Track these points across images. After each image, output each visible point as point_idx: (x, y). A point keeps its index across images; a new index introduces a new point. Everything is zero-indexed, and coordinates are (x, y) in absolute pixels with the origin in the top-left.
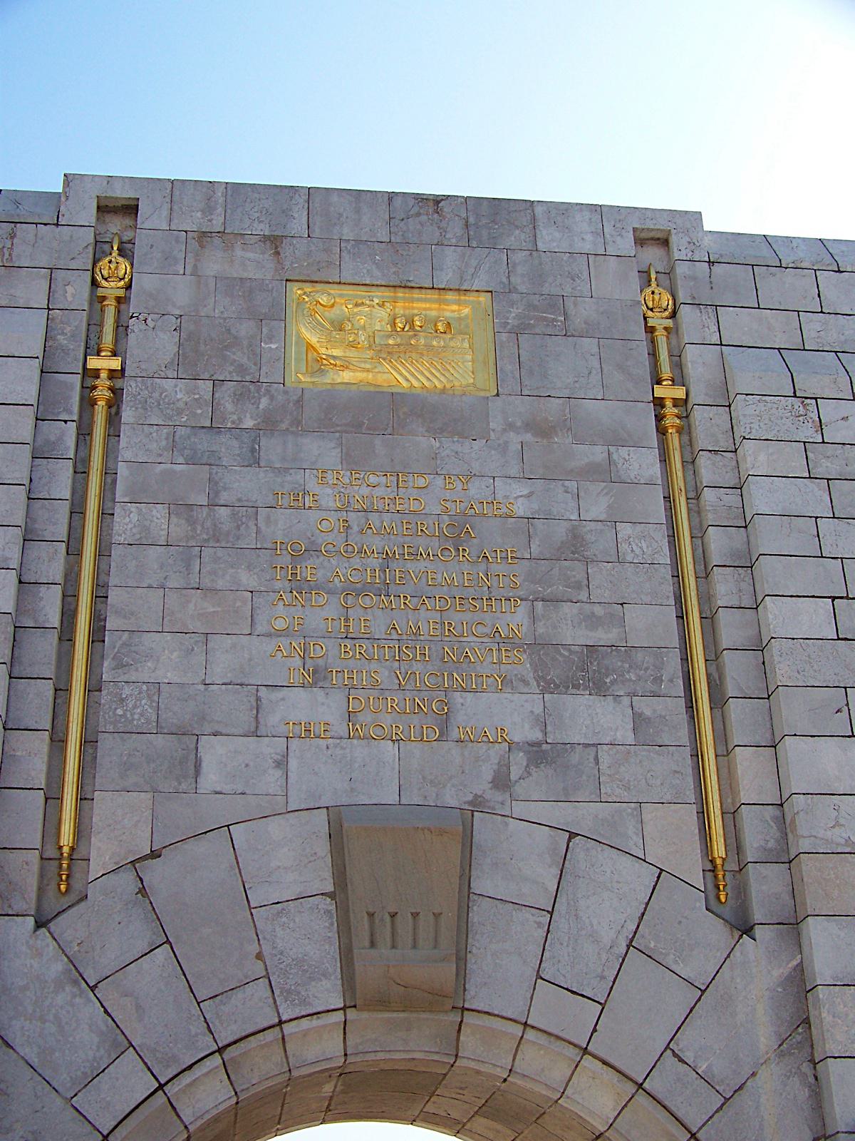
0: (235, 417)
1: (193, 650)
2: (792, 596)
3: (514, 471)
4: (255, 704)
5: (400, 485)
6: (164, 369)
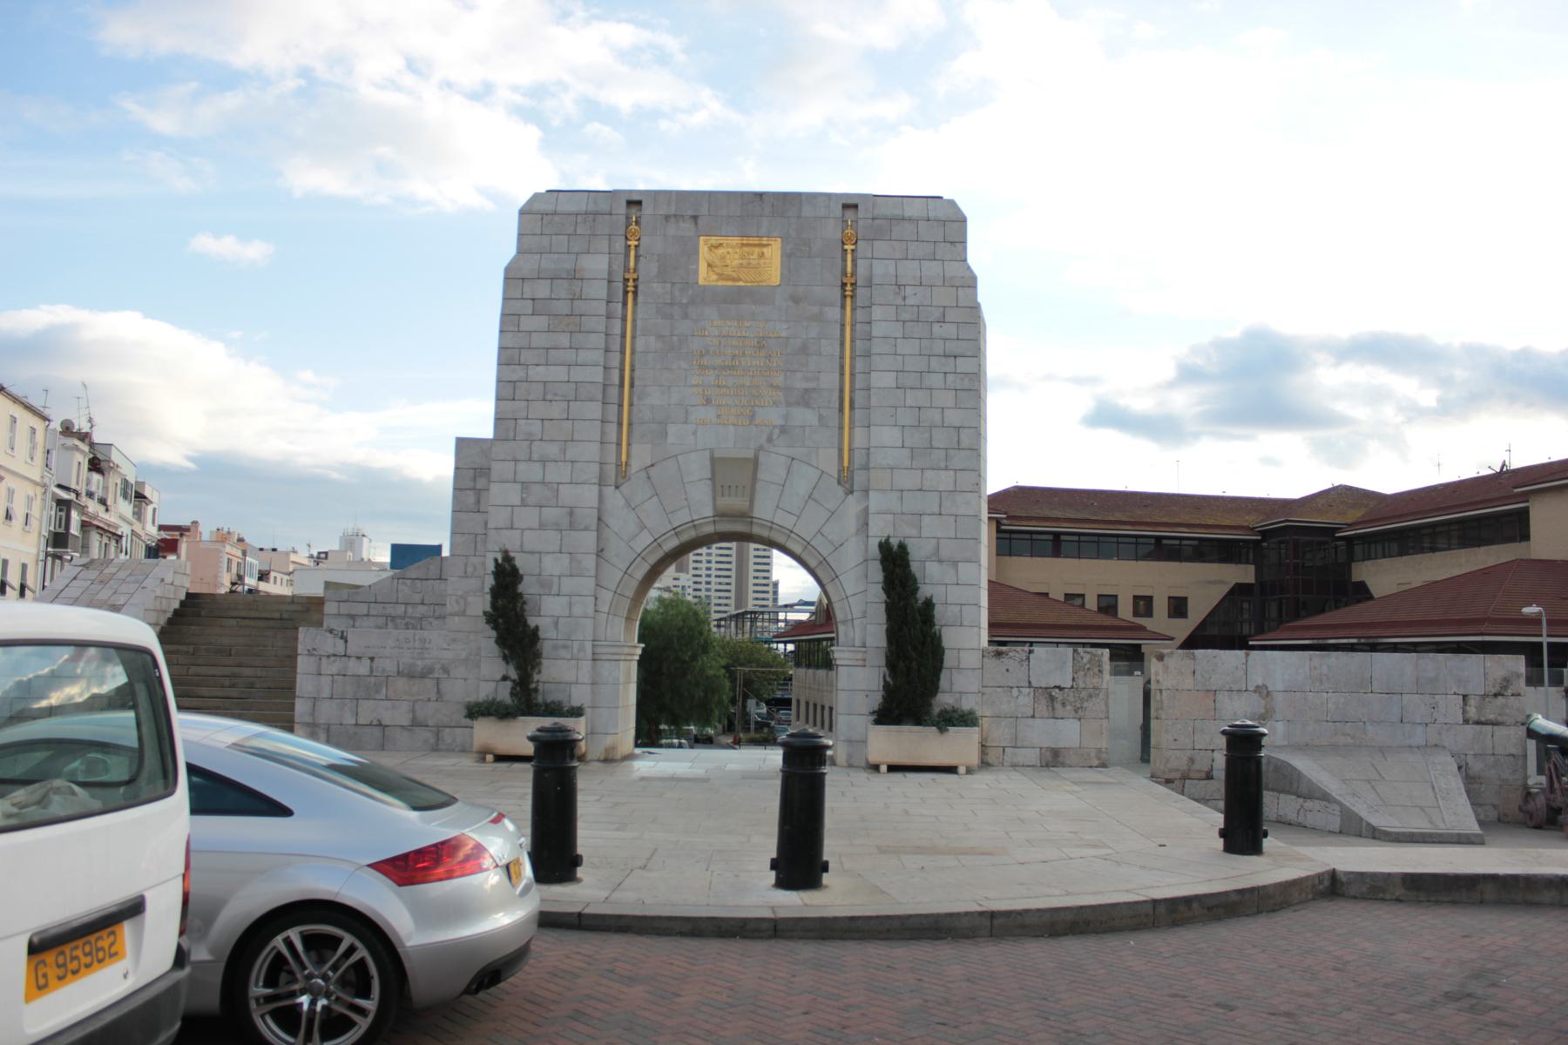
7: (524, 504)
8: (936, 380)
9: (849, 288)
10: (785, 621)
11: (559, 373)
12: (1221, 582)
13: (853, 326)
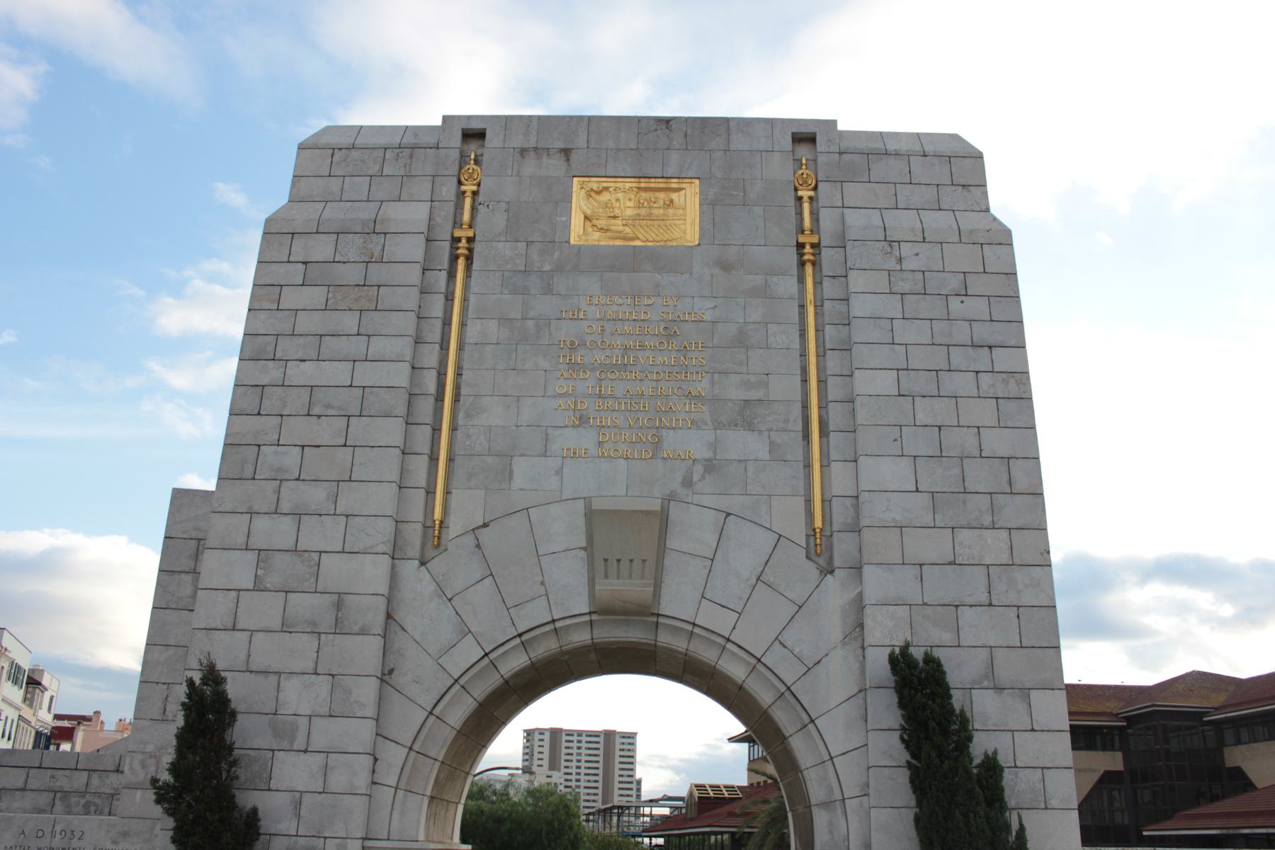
7: (259, 587)
8: (963, 384)
10: (651, 815)
11: (338, 373)
12: (1091, 770)
13: (819, 307)
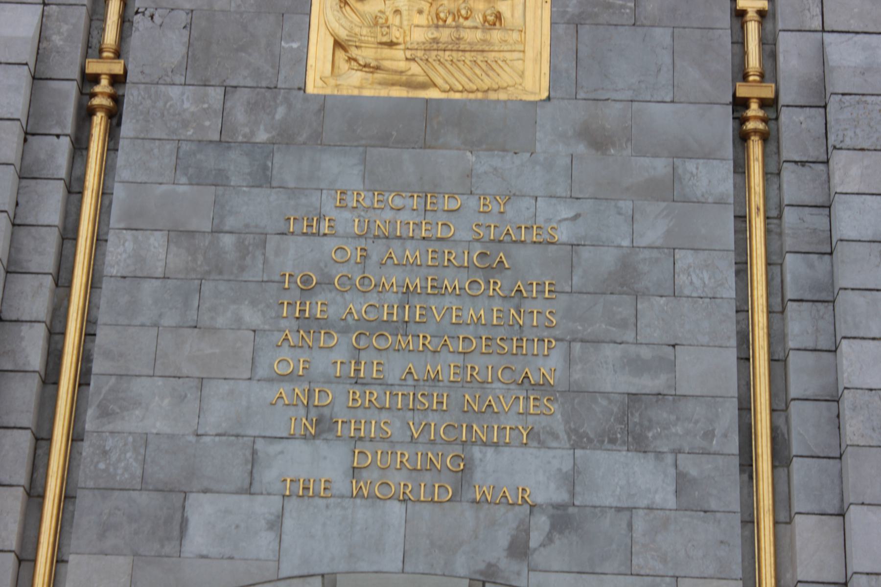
0: (247, 130)
1: (186, 396)
2: (874, 339)
3: (561, 190)
4: (250, 458)
5: (428, 207)
6: (170, 74)
9: (754, 110)
